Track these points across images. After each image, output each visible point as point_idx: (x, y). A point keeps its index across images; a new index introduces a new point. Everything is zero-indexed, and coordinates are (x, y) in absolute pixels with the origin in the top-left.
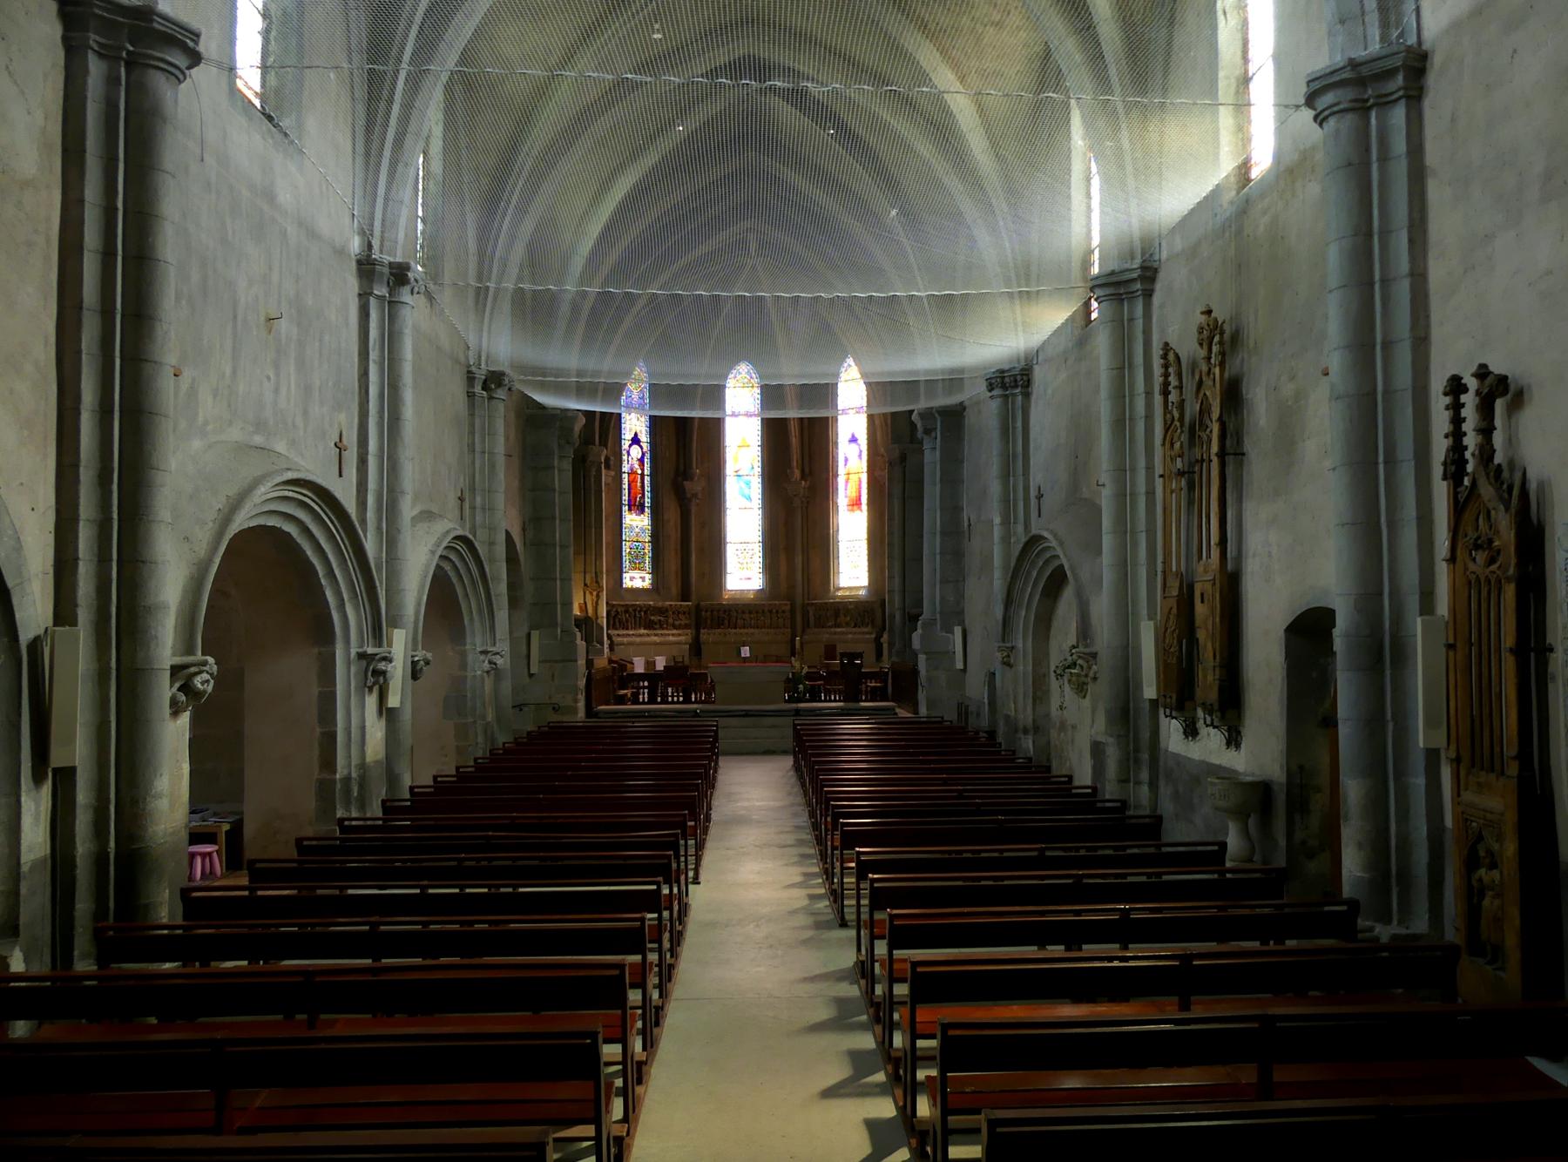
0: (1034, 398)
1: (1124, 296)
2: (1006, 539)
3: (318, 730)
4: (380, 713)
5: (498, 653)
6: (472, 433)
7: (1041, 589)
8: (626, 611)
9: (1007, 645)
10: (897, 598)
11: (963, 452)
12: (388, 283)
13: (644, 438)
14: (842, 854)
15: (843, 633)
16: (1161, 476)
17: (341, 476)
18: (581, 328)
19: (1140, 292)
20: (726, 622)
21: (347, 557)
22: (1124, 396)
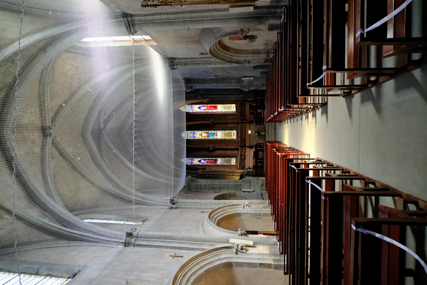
0: (176, 57)
1: (133, 23)
2: (215, 63)
3: (259, 268)
4: (255, 247)
5: (244, 204)
6: (186, 208)
7: (227, 52)
8: (241, 164)
9: (244, 62)
10: (237, 96)
12: (131, 238)
13: (199, 159)
14: (300, 104)
15: (247, 110)
16: (182, 6)
17: (183, 257)
19: (131, 18)
20: (244, 139)
21: (205, 258)
22: (162, 22)
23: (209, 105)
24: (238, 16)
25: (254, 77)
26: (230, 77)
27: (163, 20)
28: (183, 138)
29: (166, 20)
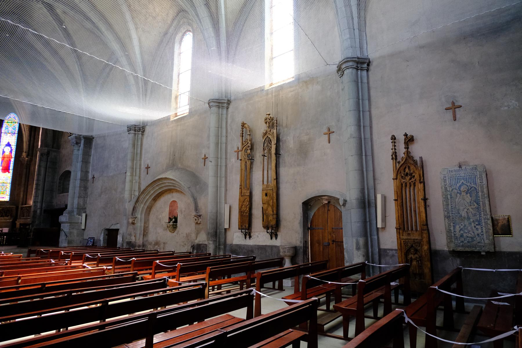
1: (221, 107)
11: (91, 153)
18: (223, 54)
19: (226, 107)
23: (13, 160)
24: (219, 213)
25: (84, 230)
26: (87, 197)
27: (221, 138)
28: (7, 115)
29: (221, 140)
